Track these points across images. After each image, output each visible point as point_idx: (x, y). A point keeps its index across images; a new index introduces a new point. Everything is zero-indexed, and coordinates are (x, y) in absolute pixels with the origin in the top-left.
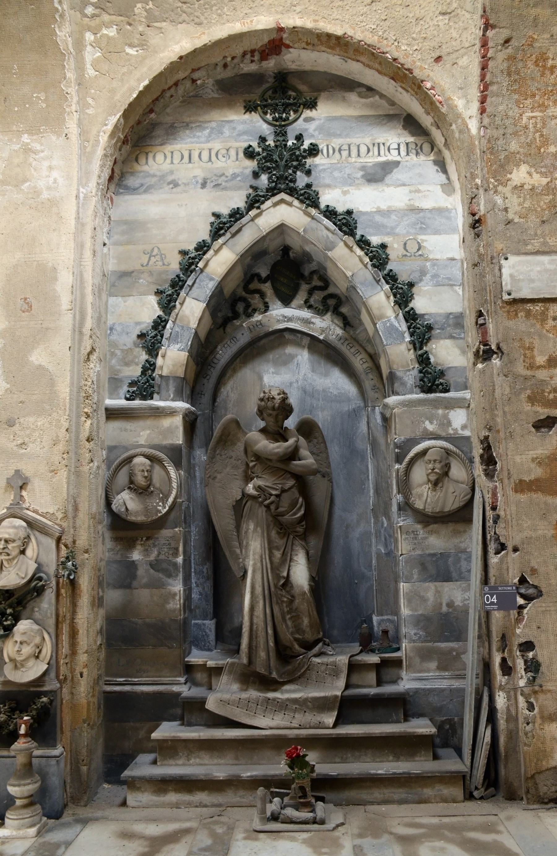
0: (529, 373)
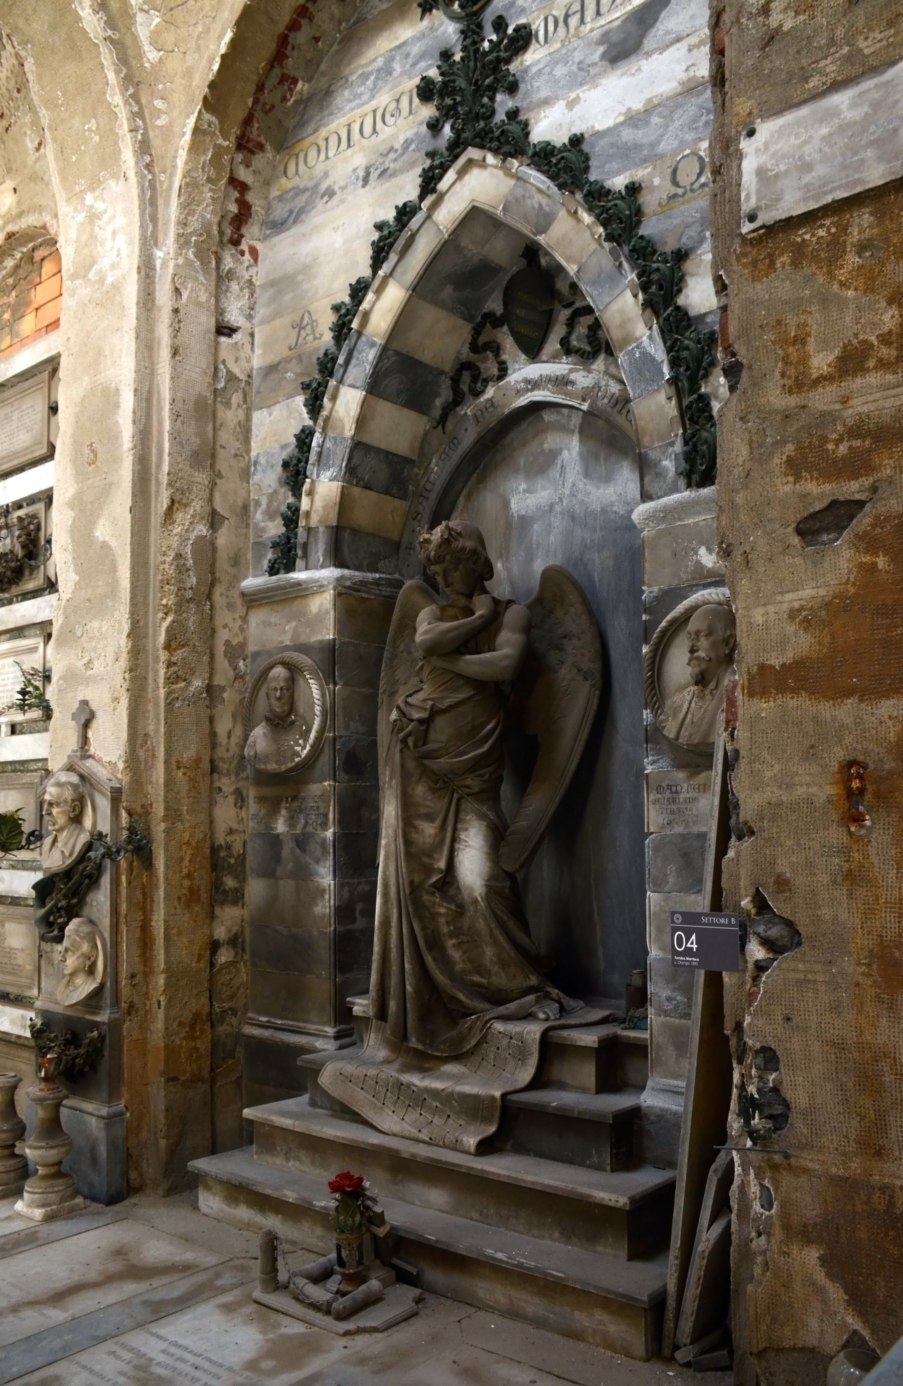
0: (792, 401)
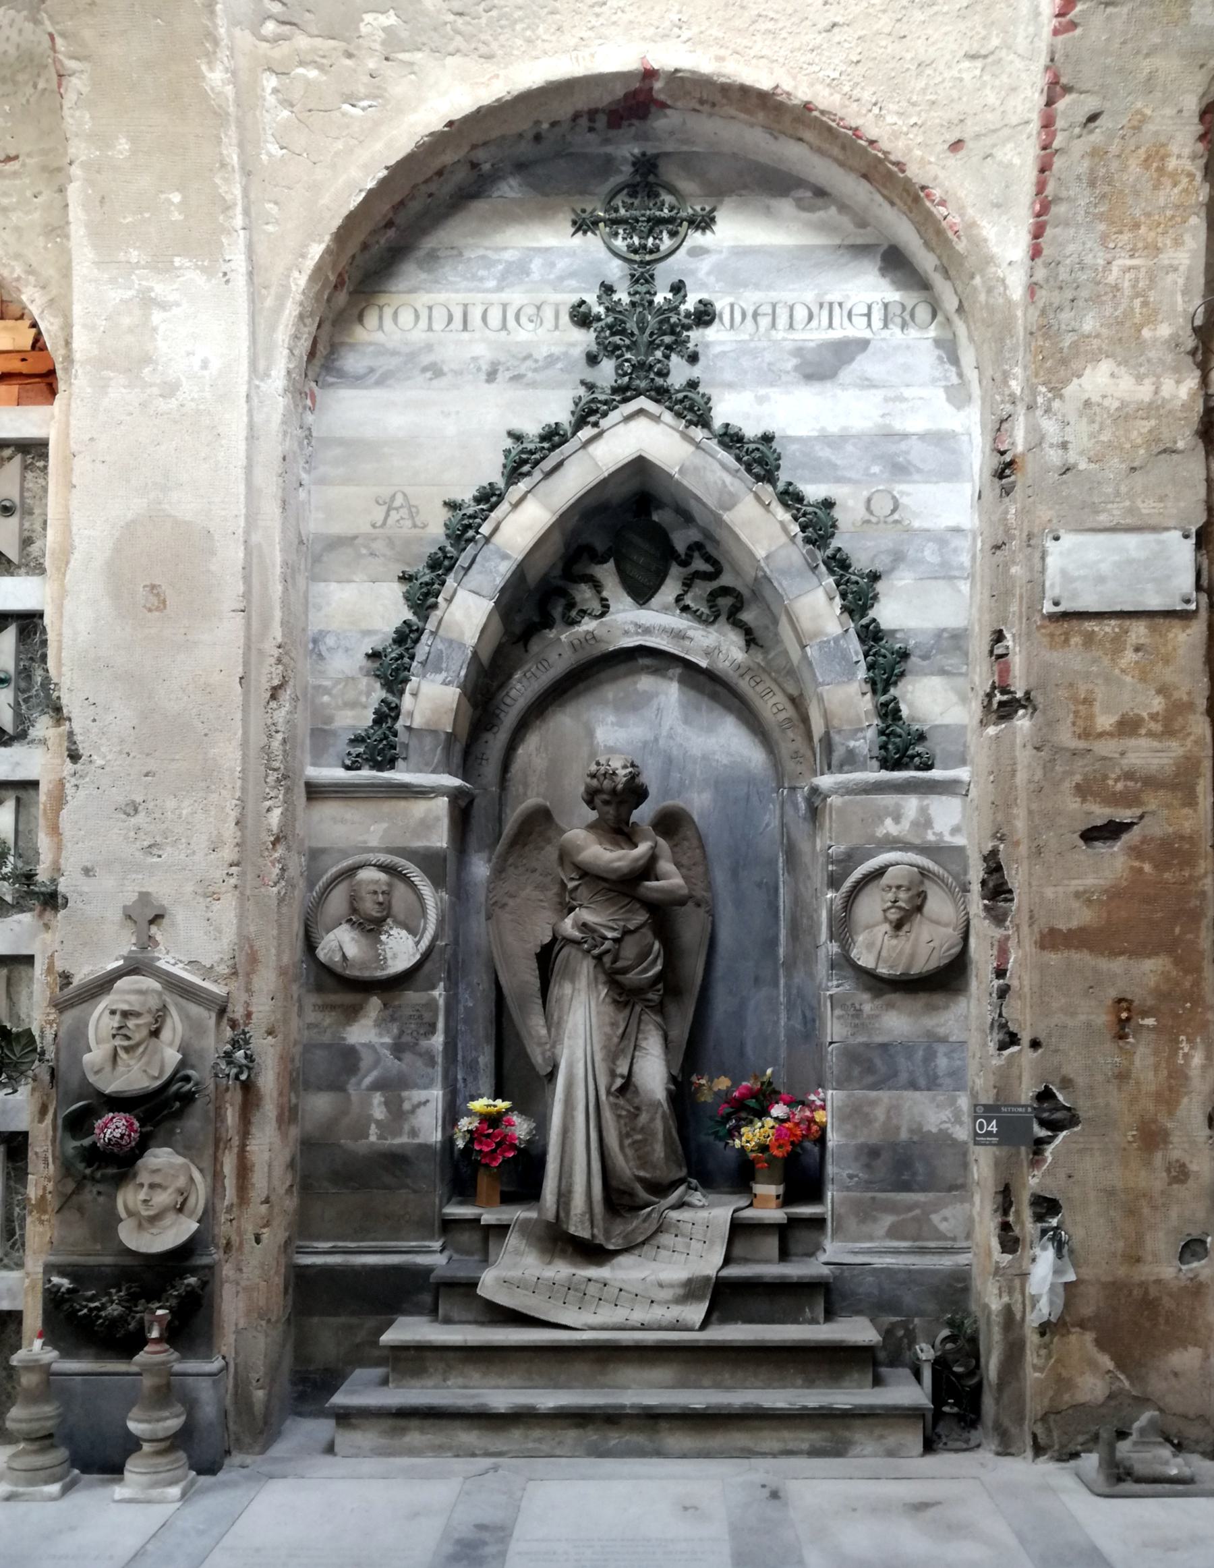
0: (1082, 744)
